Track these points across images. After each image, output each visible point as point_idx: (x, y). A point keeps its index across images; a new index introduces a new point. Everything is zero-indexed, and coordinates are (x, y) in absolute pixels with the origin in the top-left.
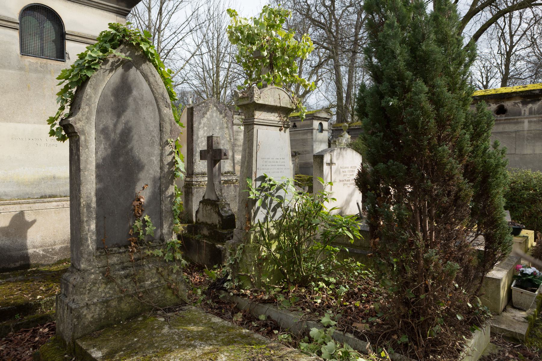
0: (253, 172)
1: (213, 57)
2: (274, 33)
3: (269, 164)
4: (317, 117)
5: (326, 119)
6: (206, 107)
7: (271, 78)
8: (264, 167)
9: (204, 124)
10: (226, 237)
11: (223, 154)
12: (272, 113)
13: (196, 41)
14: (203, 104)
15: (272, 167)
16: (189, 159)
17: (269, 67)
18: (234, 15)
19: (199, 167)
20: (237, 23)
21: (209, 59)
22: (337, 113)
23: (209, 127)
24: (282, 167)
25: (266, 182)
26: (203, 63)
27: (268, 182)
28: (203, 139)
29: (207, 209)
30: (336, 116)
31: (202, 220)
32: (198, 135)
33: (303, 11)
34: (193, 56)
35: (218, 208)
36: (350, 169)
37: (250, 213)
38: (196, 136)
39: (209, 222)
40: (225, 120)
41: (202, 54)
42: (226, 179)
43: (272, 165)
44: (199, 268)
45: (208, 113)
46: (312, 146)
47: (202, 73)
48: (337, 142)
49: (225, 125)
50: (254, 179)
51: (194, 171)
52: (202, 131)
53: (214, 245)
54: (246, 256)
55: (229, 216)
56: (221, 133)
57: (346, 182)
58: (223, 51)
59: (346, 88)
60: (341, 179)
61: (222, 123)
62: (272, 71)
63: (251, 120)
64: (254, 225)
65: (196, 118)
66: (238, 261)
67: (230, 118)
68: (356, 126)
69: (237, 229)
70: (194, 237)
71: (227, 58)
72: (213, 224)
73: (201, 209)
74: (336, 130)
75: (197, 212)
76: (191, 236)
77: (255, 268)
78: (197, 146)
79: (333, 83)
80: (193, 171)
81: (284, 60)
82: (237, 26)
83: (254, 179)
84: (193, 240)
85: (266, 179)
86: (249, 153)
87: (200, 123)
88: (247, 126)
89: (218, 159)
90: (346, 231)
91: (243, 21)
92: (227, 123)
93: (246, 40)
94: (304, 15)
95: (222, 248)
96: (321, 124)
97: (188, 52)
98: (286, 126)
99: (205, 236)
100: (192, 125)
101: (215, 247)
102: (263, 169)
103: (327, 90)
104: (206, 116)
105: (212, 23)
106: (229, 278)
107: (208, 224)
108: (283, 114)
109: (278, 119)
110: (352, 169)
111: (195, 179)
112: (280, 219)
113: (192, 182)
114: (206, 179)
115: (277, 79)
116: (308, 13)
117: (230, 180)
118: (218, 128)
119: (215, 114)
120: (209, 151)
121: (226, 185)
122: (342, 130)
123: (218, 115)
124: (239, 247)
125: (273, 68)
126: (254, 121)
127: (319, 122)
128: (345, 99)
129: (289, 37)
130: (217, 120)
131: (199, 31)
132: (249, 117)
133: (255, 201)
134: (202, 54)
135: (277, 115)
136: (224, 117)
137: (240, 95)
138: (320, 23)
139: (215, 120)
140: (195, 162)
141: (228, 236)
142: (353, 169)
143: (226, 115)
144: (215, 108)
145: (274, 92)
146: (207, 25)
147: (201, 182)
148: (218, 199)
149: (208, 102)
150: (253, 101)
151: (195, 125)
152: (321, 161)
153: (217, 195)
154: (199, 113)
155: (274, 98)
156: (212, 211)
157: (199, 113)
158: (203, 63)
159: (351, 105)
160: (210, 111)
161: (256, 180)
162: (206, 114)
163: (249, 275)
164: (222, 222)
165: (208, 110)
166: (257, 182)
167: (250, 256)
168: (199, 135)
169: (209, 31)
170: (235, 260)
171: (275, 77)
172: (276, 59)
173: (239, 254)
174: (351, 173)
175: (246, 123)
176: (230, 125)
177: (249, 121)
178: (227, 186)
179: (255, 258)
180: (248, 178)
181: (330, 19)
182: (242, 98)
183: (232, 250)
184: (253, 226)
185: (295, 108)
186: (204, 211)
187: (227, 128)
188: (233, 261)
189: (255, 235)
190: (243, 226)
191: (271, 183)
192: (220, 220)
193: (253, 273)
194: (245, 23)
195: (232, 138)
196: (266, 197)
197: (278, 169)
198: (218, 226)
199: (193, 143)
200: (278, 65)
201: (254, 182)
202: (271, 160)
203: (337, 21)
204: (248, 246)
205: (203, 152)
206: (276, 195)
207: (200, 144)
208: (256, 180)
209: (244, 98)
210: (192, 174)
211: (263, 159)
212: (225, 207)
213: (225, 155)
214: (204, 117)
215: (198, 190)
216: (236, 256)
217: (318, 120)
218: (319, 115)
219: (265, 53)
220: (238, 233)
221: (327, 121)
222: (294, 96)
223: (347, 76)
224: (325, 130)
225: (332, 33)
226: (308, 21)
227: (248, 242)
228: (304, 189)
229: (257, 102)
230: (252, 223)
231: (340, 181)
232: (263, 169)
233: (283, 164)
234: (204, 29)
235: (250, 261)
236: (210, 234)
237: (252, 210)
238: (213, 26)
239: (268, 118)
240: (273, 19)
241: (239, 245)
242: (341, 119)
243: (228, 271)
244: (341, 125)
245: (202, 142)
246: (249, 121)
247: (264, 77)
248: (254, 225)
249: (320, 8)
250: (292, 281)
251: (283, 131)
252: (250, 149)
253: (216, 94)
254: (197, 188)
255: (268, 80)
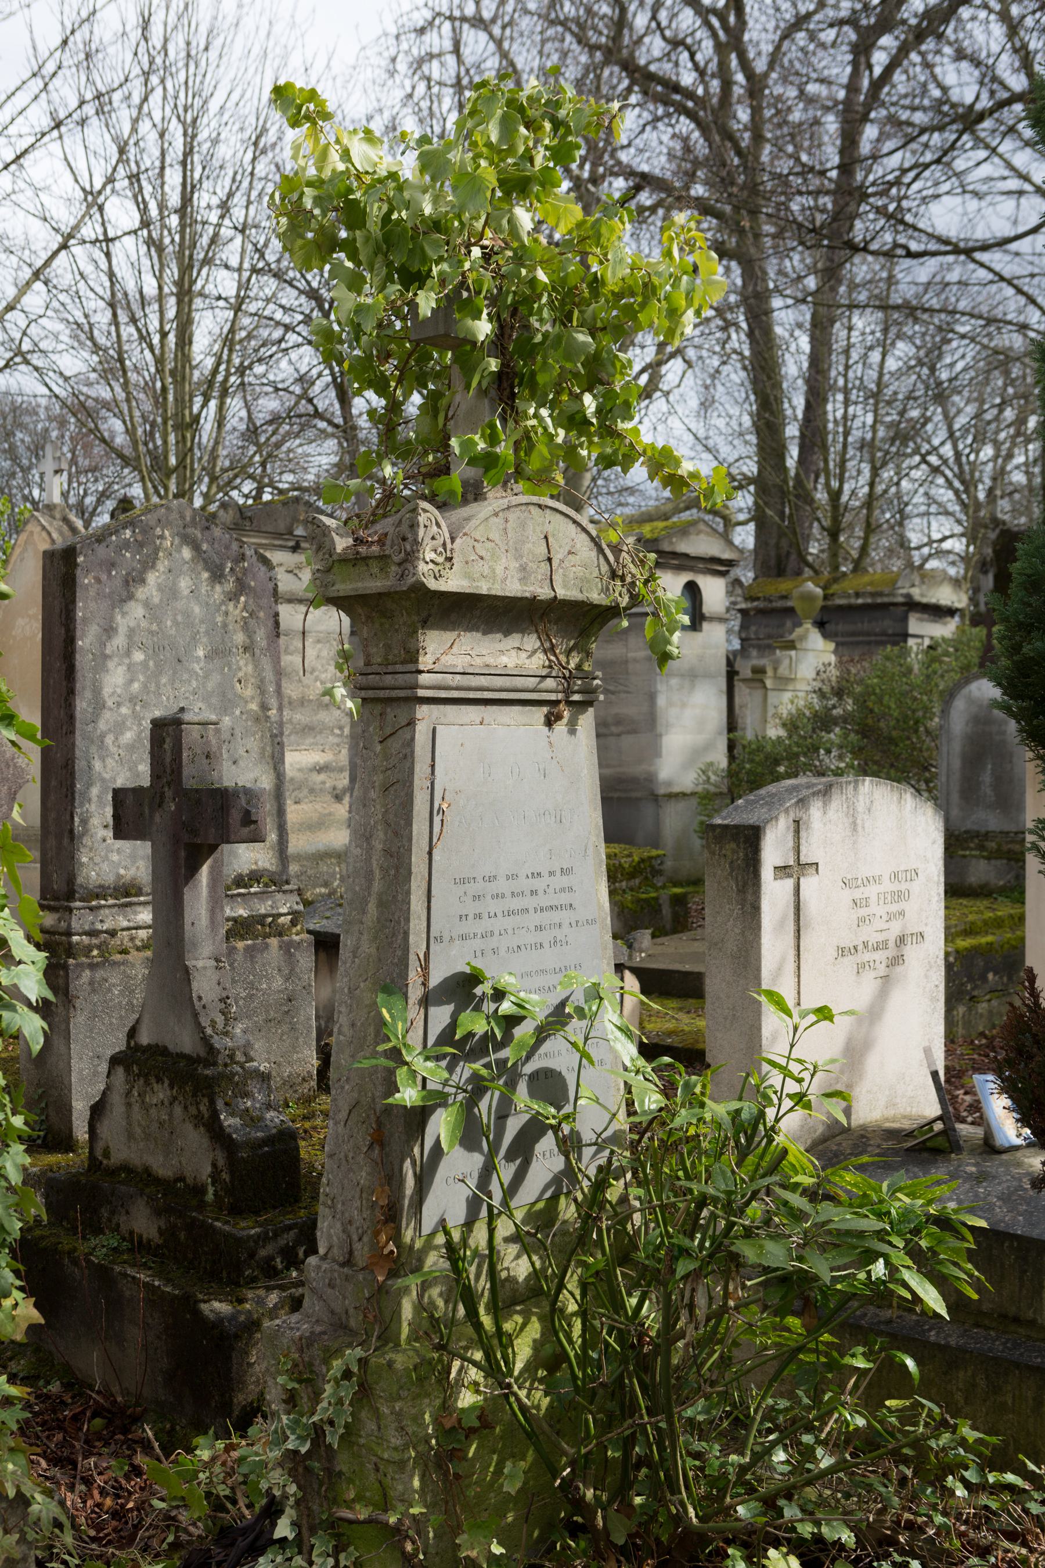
0: (412, 957)
1: (160, 249)
2: (524, 218)
3: (494, 906)
4: (675, 555)
5: (717, 566)
6: (141, 545)
7: (504, 449)
8: (470, 927)
9: (131, 632)
10: (252, 1255)
11: (235, 816)
12: (507, 633)
13: (81, 166)
14: (128, 533)
15: (509, 922)
16: (53, 815)
17: (493, 393)
18: (308, 118)
19: (106, 858)
20: (323, 157)
21: (146, 263)
22: (759, 518)
23: (155, 651)
24: (556, 916)
25: (477, 1009)
26: (111, 275)
27: (489, 1007)
28: (124, 710)
29: (151, 1099)
30: (751, 527)
31: (122, 1152)
32: (97, 691)
33: (595, 28)
34: (64, 246)
35: (212, 1102)
36: (887, 886)
37: (394, 1179)
38: (88, 694)
39: (162, 1167)
40: (236, 611)
41: (108, 240)
42: (242, 912)
43: (510, 913)
44: (110, 1422)
45: (152, 578)
46: (652, 697)
47: (102, 318)
48: (770, 672)
49: (240, 638)
50: (415, 993)
51: (80, 880)
52: (121, 670)
53: (189, 1304)
54: (378, 1416)
55: (264, 1142)
56: (216, 678)
57: (867, 956)
58: (213, 218)
59: (799, 401)
60: (848, 943)
61: (225, 625)
62: (511, 412)
63: (401, 679)
64: (418, 1244)
65: (92, 605)
66: (332, 1439)
67: (264, 602)
68: (857, 595)
69: (324, 1258)
70: (83, 1248)
71: (232, 252)
72: (182, 1179)
73: (116, 1099)
74: (760, 612)
75: (97, 1111)
76: (66, 1243)
77: (422, 1480)
78: (93, 749)
79: (736, 375)
80: (71, 880)
81: (571, 351)
82: (327, 174)
83: (415, 993)
84: (75, 1262)
85: (478, 991)
86: (387, 852)
87: (110, 630)
88: (378, 709)
89: (211, 841)
90: (906, 1275)
91: (359, 150)
92: (246, 628)
93: (380, 258)
94: (597, 47)
95: (233, 1317)
96: (692, 590)
97: (38, 223)
98: (576, 697)
99: (138, 1247)
100: (70, 641)
101: (197, 1313)
102: (463, 937)
103: (706, 405)
104: (141, 593)
105: (159, 91)
106: (283, 1529)
107: (157, 1181)
108: (565, 634)
109: (538, 661)
110: (895, 887)
111: (81, 920)
112: (548, 1195)
113: (69, 934)
114: (145, 916)
115: (534, 455)
116: (617, 37)
117: (261, 919)
118: (201, 653)
119: (184, 584)
120: (162, 796)
121: (240, 945)
122: (790, 611)
123: (204, 589)
124: (337, 1364)
125: (513, 396)
126: (416, 686)
127: (684, 578)
128: (794, 451)
129: (598, 236)
130: (197, 610)
131: (94, 121)
132: (387, 663)
133: (419, 1117)
134: (108, 240)
135: (531, 642)
136: (233, 597)
137: (342, 543)
138: (676, 88)
139: (187, 614)
140: (86, 831)
141: (263, 1253)
142: (903, 887)
143: (242, 587)
144: (187, 553)
145: (523, 525)
146: (136, 99)
147: (112, 933)
148: (211, 1049)
149: (150, 519)
150: (411, 580)
151: (86, 641)
152: (746, 858)
153: (202, 1030)
154: (104, 577)
155: (518, 556)
156: (178, 1110)
157: (104, 577)
158: (111, 275)
159: (827, 484)
160: (162, 565)
161: (426, 1002)
162: (143, 581)
163: (392, 1520)
164: (232, 1173)
165: (150, 563)
166: (432, 1010)
167: (399, 1415)
168: (106, 691)
169: (145, 126)
170: (318, 1433)
171: (525, 443)
172: (529, 350)
173: (340, 1402)
174: (894, 908)
175: (370, 694)
176: (261, 636)
177: (389, 680)
178: (247, 948)
179: (424, 1427)
180: (387, 990)
181: (724, 66)
182: (354, 560)
183: (300, 1381)
184: (411, 1247)
185: (624, 601)
186: (136, 1108)
187: (246, 649)
188: (302, 1439)
189: (420, 1296)
190: (357, 1246)
191: (506, 1007)
192: (221, 1163)
193: (415, 1511)
194: (368, 159)
195: (273, 702)
196: (478, 1088)
197: (539, 928)
198: (210, 1196)
199: (72, 732)
200: (541, 379)
201: (414, 1012)
202: (502, 885)
203: (756, 85)
204: (390, 1364)
205: (130, 800)
206: (529, 1069)
207: (109, 740)
208: (426, 1002)
209: (365, 559)
210: (70, 895)
211: (463, 881)
212: (246, 1095)
213: (248, 819)
214: (131, 597)
215: (100, 974)
216: (323, 1410)
217: (680, 568)
218: (684, 546)
219: (483, 328)
220: (331, 1285)
221: (723, 574)
222: (621, 541)
223: (804, 342)
224: (711, 619)
225: (729, 136)
226: (614, 76)
227: (388, 1337)
228: (630, 946)
229: (432, 585)
230: (408, 1235)
231: (842, 951)
232: (463, 937)
233: (564, 898)
234: (123, 118)
235: (396, 1441)
236: (169, 1233)
237: (408, 1163)
238: (165, 98)
239: (491, 661)
240: (521, 149)
241: (338, 1352)
242: (777, 546)
243: (277, 1493)
244: (784, 585)
245: (119, 728)
246: (389, 680)
247: (467, 445)
248: (418, 1244)
249: (673, 16)
250: (621, 1542)
251: (561, 727)
252: (396, 834)
253: (176, 428)
254: (92, 967)
255: (488, 462)
